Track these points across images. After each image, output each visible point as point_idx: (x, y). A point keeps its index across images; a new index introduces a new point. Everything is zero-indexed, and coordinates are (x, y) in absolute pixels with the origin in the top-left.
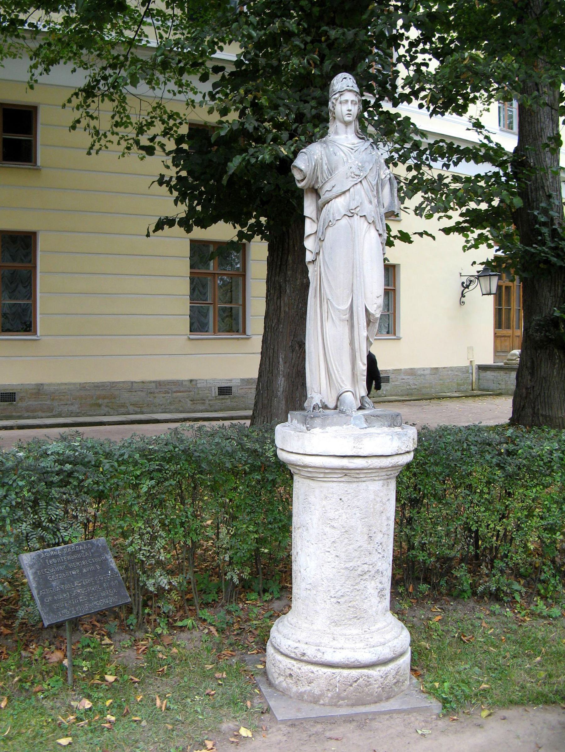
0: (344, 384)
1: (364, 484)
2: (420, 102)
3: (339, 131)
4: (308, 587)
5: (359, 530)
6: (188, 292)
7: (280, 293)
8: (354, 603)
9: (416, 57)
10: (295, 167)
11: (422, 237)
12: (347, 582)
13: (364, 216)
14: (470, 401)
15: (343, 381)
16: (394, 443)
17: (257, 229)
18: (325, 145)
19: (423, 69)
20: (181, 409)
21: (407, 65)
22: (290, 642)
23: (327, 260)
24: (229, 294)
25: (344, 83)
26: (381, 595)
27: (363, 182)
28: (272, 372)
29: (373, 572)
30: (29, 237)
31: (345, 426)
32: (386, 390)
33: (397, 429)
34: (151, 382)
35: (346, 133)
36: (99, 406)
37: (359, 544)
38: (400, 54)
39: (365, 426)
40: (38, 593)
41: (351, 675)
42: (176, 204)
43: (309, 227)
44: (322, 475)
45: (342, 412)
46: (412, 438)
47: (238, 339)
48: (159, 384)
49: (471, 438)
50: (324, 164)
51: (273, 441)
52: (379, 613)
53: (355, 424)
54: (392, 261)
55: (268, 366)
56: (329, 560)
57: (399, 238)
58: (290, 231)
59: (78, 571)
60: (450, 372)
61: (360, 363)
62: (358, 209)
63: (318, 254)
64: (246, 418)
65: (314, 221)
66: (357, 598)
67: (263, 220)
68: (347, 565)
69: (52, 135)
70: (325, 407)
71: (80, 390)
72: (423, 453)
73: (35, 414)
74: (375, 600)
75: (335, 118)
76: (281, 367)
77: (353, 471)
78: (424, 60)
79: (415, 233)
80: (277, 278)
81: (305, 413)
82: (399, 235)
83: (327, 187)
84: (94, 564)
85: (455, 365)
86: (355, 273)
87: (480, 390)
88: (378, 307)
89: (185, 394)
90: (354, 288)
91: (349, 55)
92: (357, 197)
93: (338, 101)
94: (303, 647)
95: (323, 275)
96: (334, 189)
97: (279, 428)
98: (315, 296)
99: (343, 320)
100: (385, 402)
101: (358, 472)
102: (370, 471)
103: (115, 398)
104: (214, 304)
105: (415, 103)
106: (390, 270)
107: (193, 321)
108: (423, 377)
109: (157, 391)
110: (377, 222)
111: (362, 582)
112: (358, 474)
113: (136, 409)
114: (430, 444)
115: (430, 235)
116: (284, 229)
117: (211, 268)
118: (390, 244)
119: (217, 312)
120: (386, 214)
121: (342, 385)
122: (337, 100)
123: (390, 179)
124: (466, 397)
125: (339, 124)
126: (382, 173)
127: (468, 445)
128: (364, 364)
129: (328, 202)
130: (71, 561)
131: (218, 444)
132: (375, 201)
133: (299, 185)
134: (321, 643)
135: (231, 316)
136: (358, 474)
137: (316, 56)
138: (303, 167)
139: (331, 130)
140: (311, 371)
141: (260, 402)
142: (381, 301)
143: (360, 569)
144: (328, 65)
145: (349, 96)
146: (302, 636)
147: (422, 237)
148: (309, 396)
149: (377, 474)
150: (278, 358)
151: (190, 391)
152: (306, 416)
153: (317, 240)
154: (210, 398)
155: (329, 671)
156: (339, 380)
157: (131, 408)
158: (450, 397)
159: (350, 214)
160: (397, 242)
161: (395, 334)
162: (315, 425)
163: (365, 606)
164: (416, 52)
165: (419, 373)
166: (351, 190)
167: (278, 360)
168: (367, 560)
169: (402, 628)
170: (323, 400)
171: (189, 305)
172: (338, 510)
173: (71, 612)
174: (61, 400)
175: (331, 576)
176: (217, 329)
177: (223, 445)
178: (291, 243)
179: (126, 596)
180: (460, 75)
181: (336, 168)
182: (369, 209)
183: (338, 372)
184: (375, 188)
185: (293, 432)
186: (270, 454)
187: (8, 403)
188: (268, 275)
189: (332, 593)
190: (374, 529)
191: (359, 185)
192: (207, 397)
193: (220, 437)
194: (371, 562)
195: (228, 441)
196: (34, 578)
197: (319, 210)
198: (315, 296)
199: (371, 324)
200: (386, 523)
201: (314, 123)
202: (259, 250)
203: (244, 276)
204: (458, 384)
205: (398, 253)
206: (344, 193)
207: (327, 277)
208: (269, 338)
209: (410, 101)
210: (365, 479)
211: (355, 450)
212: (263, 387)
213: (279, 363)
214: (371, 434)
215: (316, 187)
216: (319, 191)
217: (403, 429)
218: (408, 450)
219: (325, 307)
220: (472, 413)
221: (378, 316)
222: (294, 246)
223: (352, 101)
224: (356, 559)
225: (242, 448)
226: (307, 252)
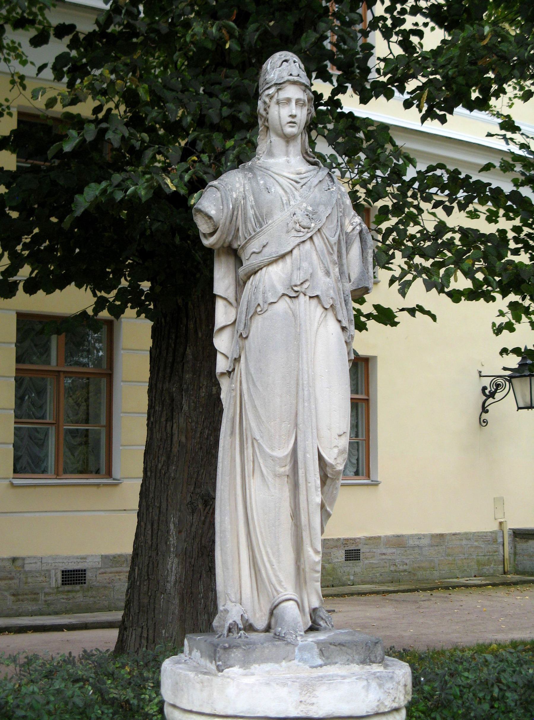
2: (407, 96)
3: (275, 151)
6: (12, 404)
7: (172, 411)
9: (404, 21)
10: (199, 211)
11: (414, 316)
13: (317, 296)
14: (501, 594)
15: (280, 582)
17: (132, 297)
18: (250, 175)
19: (415, 39)
21: (387, 34)
23: (252, 370)
24: (83, 408)
25: (283, 67)
27: (315, 238)
28: (157, 549)
31: (284, 663)
32: (355, 574)
33: (376, 668)
35: (287, 154)
38: (377, 14)
39: (320, 662)
43: (223, 314)
45: (278, 637)
46: (402, 683)
47: (98, 485)
49: (506, 678)
50: (249, 208)
51: (157, 685)
53: (301, 660)
54: (362, 352)
55: (149, 537)
58: (190, 305)
60: (464, 542)
62: (306, 286)
63: (237, 360)
64: (109, 625)
65: (230, 303)
67: (146, 285)
70: (249, 628)
72: (421, 706)
75: (268, 128)
76: (173, 540)
78: (416, 24)
79: (403, 310)
80: (167, 385)
81: (215, 639)
82: (375, 313)
83: (254, 246)
85: (473, 529)
86: (300, 393)
87: (517, 572)
88: (341, 452)
90: (300, 420)
91: (289, 18)
92: (305, 265)
93: (274, 100)
95: (246, 397)
96: (266, 250)
97: (167, 665)
98: (232, 433)
99: (280, 476)
100: (352, 594)
104: (57, 424)
105: (399, 98)
106: (361, 368)
107: (19, 454)
108: (417, 550)
110: (338, 306)
114: (434, 689)
115: (428, 313)
116: (180, 301)
117: (54, 361)
118: (361, 327)
119: (62, 441)
120: (353, 292)
121: (279, 588)
122: (271, 97)
123: (361, 232)
124: (494, 585)
125: (274, 138)
126: (347, 222)
127: (501, 690)
128: (317, 552)
129: (256, 273)
131: (59, 691)
133: (207, 242)
135: (86, 443)
137: (232, 24)
138: (212, 212)
139: (262, 148)
140: (224, 563)
141: (136, 603)
142: (344, 442)
144: (252, 33)
145: (293, 92)
147: (414, 316)
148: (221, 608)
150: (167, 523)
151: (11, 579)
152: (215, 646)
153: (237, 336)
154: (47, 590)
158: (467, 586)
159: (293, 294)
160: (371, 324)
161: (368, 476)
162: (231, 662)
164: (403, 12)
165: (411, 543)
166: (295, 252)
167: (168, 526)
170: (246, 616)
171: (13, 426)
176: (61, 469)
177: (69, 693)
178: (191, 326)
180: (477, 59)
181: (269, 214)
182: (325, 284)
183: (272, 565)
184: (335, 249)
185: (192, 675)
186: (152, 709)
188: (151, 379)
191: (308, 245)
192: (43, 588)
193: (64, 680)
195: (78, 685)
197: (240, 284)
198: (232, 433)
199: (328, 482)
201: (234, 133)
202: (136, 334)
203: (110, 376)
204: (478, 563)
205: (373, 339)
206: (283, 257)
207: (254, 407)
208: (152, 488)
209: (389, 95)
211: (302, 707)
212: (140, 575)
213: (168, 532)
214: (330, 678)
215: (235, 246)
216: (240, 252)
217: (386, 666)
218: (395, 705)
219: (249, 452)
220: (506, 616)
221: (341, 467)
222: (196, 332)
223: (297, 101)
225: (103, 698)
226: (219, 357)
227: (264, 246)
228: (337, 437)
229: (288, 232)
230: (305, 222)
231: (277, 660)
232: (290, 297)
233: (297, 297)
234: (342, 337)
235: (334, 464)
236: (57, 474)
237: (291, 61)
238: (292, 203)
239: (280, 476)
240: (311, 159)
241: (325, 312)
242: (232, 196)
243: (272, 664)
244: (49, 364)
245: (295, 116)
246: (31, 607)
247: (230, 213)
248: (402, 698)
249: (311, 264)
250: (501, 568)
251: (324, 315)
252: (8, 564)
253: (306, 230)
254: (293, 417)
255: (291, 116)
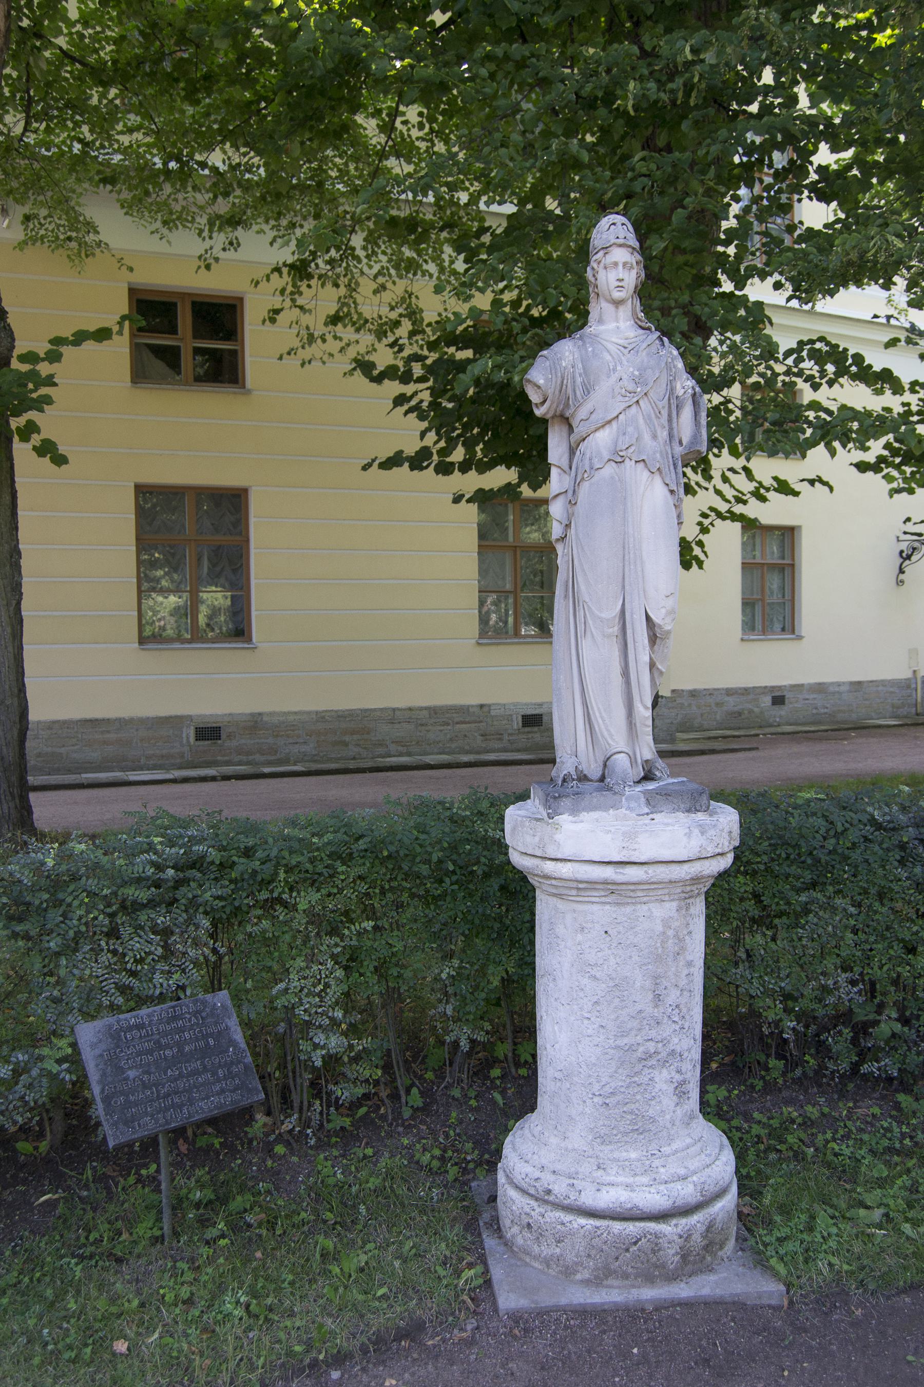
0: (613, 740)
1: (645, 907)
4: (558, 1075)
5: (638, 984)
8: (633, 1106)
10: (529, 381)
12: (620, 1071)
15: (611, 735)
16: (702, 839)
18: (580, 343)
20: (467, 747)
22: (528, 1169)
23: (581, 536)
26: (680, 1091)
29: (664, 1054)
30: (239, 496)
31: (611, 811)
32: (781, 717)
33: (700, 816)
34: (421, 709)
36: (346, 744)
37: (638, 1007)
39: (646, 810)
40: (102, 1091)
41: (627, 1231)
44: (574, 892)
45: (609, 789)
46: (727, 830)
48: (434, 711)
52: (677, 1123)
53: (629, 808)
56: (590, 1032)
57: (775, 490)
59: (175, 1050)
60: (880, 688)
61: (639, 705)
63: (568, 526)
66: (638, 1097)
68: (619, 1042)
69: (261, 345)
70: (583, 778)
71: (317, 721)
73: (251, 758)
74: (669, 1102)
77: (624, 887)
83: (582, 413)
84: (205, 1037)
85: (889, 678)
89: (473, 725)
92: (630, 430)
93: (602, 265)
94: (547, 1179)
96: (593, 416)
98: (566, 596)
99: (609, 636)
101: (632, 887)
102: (653, 887)
103: (368, 733)
109: (432, 721)
111: (646, 1071)
112: (633, 891)
113: (400, 748)
125: (604, 304)
126: (678, 386)
128: (646, 708)
130: (165, 1034)
132: (663, 434)
134: (577, 1173)
136: (633, 891)
139: (592, 317)
143: (641, 1049)
146: (546, 1157)
149: (666, 891)
155: (590, 1223)
156: (606, 733)
157: (393, 748)
158: (880, 727)
159: (618, 459)
161: (793, 632)
162: (561, 810)
163: (651, 1112)
165: (831, 689)
166: (621, 417)
168: (653, 1034)
169: (722, 1147)
172: (601, 950)
173: (157, 1121)
174: (288, 736)
175: (593, 1060)
179: (257, 1089)
183: (603, 721)
187: (207, 742)
189: (596, 1088)
190: (665, 983)
191: (634, 409)
194: (659, 1038)
196: (97, 1065)
198: (566, 596)
200: (685, 972)
204: (893, 706)
206: (609, 422)
207: (583, 570)
210: (645, 899)
211: (625, 852)
215: (567, 415)
216: (571, 420)
223: (625, 264)
224: (634, 1033)
229: (613, 397)
230: (631, 387)
231: (606, 809)
234: (670, 500)
236: (764, 633)
237: (619, 224)
238: (619, 368)
239: (609, 636)
240: (643, 324)
242: (560, 365)
243: (595, 815)
244: (507, 540)
246: (497, 745)
247: (559, 382)
248: (727, 844)
249: (637, 428)
250: (913, 710)
252: (476, 710)
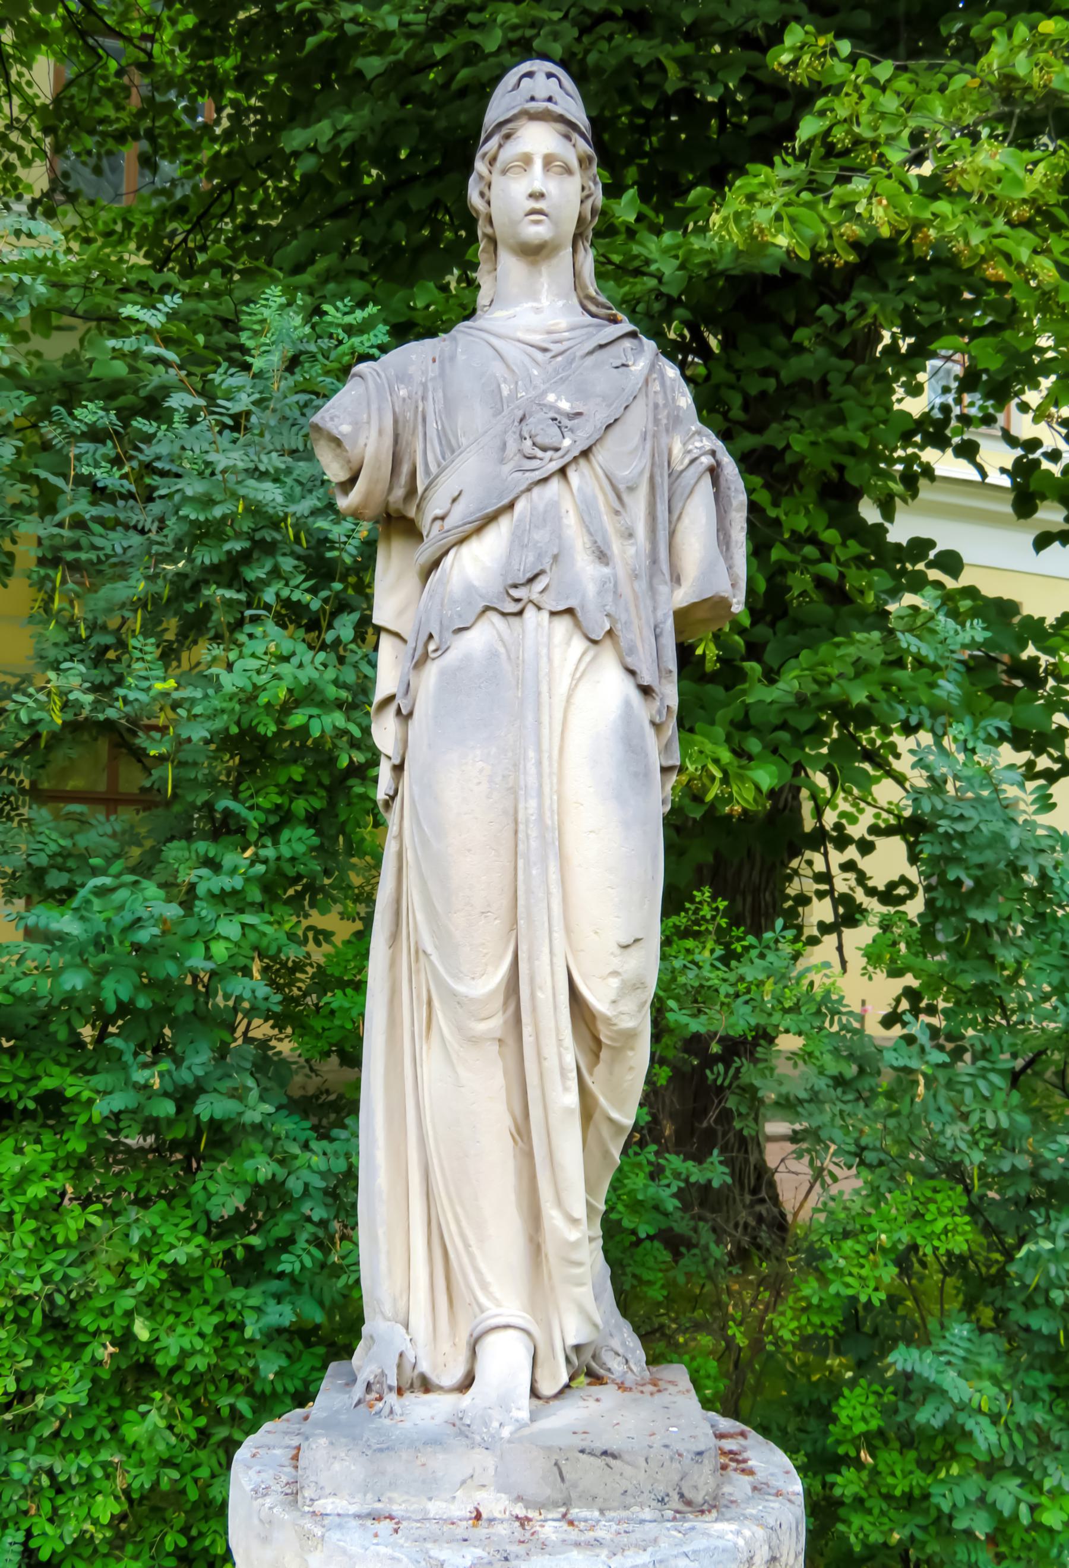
13: (570, 611)
42: (1054, 805)
83: (436, 506)
99: (474, 1040)
122: (493, 161)
125: (509, 264)
128: (574, 1221)
132: (629, 553)
159: (512, 600)
166: (519, 507)
170: (410, 1356)
191: (555, 484)
199: (604, 1054)
223: (548, 161)
227: (454, 500)
228: (618, 951)
232: (504, 614)
233: (520, 613)
235: (609, 1013)
241: (593, 650)
245: (542, 195)
251: (587, 658)
253: (550, 453)
254: (505, 901)
255: (531, 196)
